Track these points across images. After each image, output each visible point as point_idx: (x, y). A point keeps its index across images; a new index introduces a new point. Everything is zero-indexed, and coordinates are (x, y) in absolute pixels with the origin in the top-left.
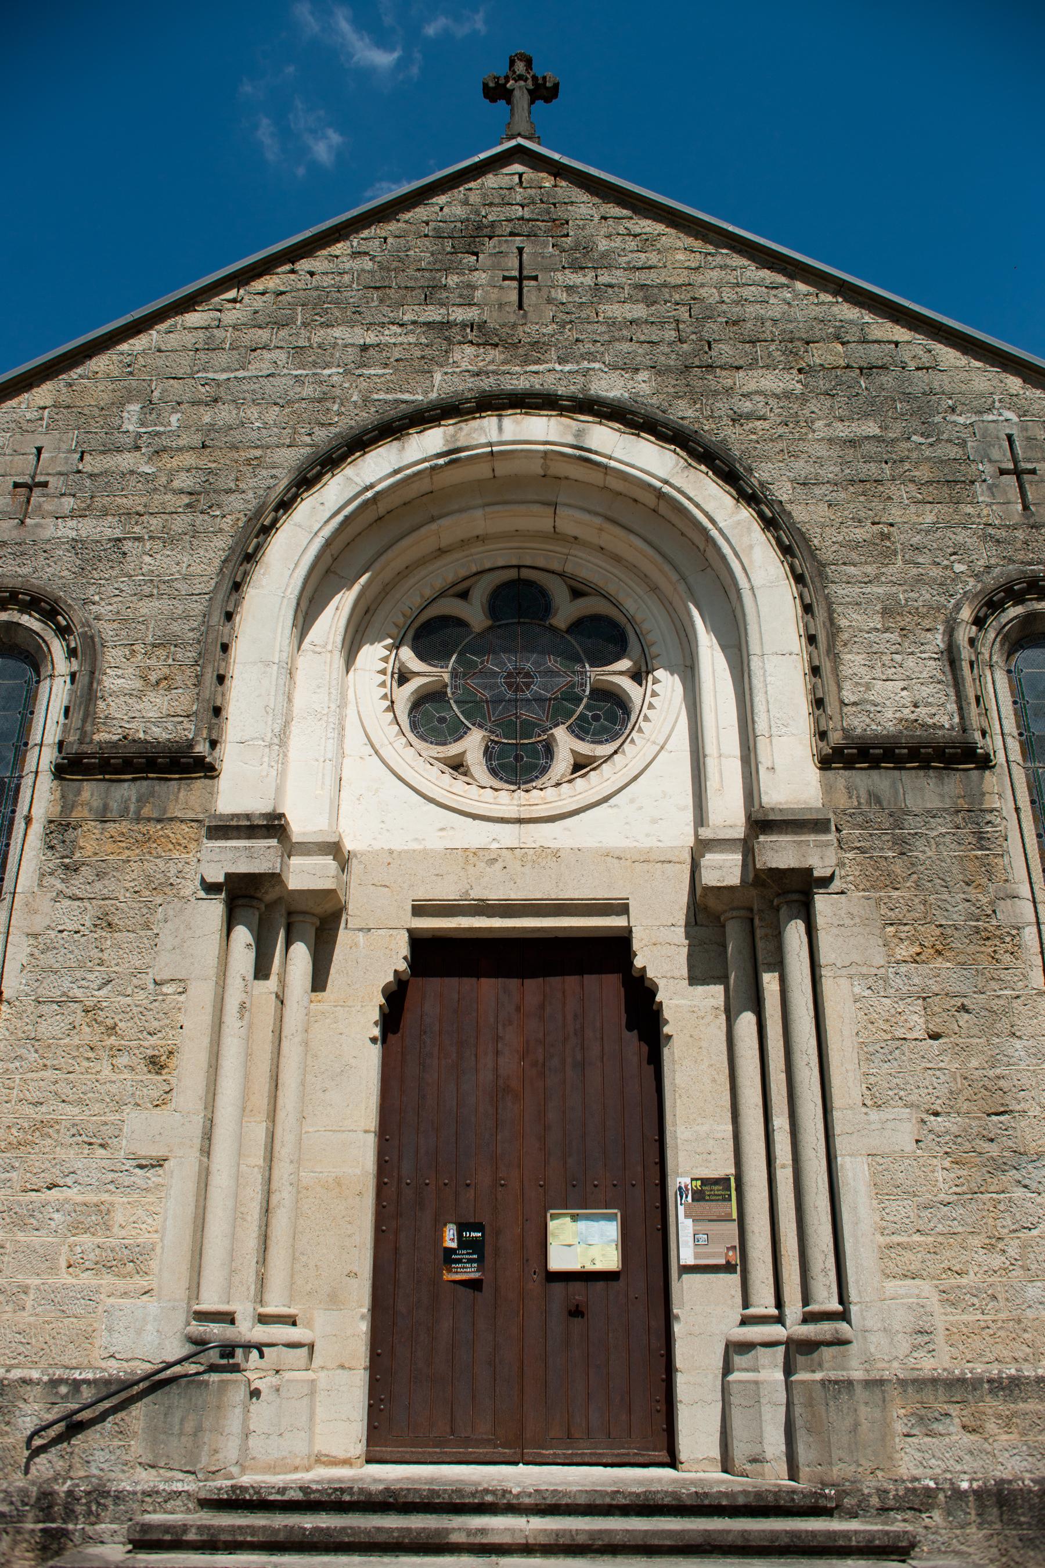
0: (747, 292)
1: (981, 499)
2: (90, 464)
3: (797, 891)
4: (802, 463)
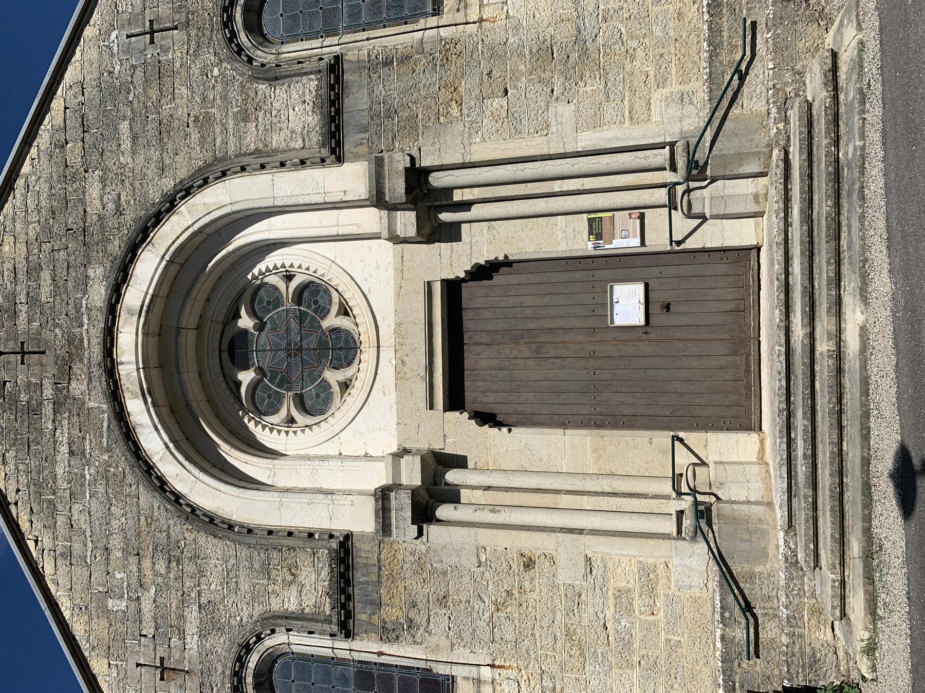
0: (31, 204)
1: (171, 57)
2: (149, 630)
3: (417, 176)
4: (149, 171)
